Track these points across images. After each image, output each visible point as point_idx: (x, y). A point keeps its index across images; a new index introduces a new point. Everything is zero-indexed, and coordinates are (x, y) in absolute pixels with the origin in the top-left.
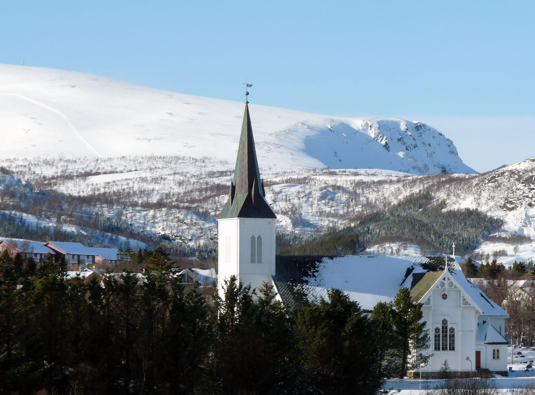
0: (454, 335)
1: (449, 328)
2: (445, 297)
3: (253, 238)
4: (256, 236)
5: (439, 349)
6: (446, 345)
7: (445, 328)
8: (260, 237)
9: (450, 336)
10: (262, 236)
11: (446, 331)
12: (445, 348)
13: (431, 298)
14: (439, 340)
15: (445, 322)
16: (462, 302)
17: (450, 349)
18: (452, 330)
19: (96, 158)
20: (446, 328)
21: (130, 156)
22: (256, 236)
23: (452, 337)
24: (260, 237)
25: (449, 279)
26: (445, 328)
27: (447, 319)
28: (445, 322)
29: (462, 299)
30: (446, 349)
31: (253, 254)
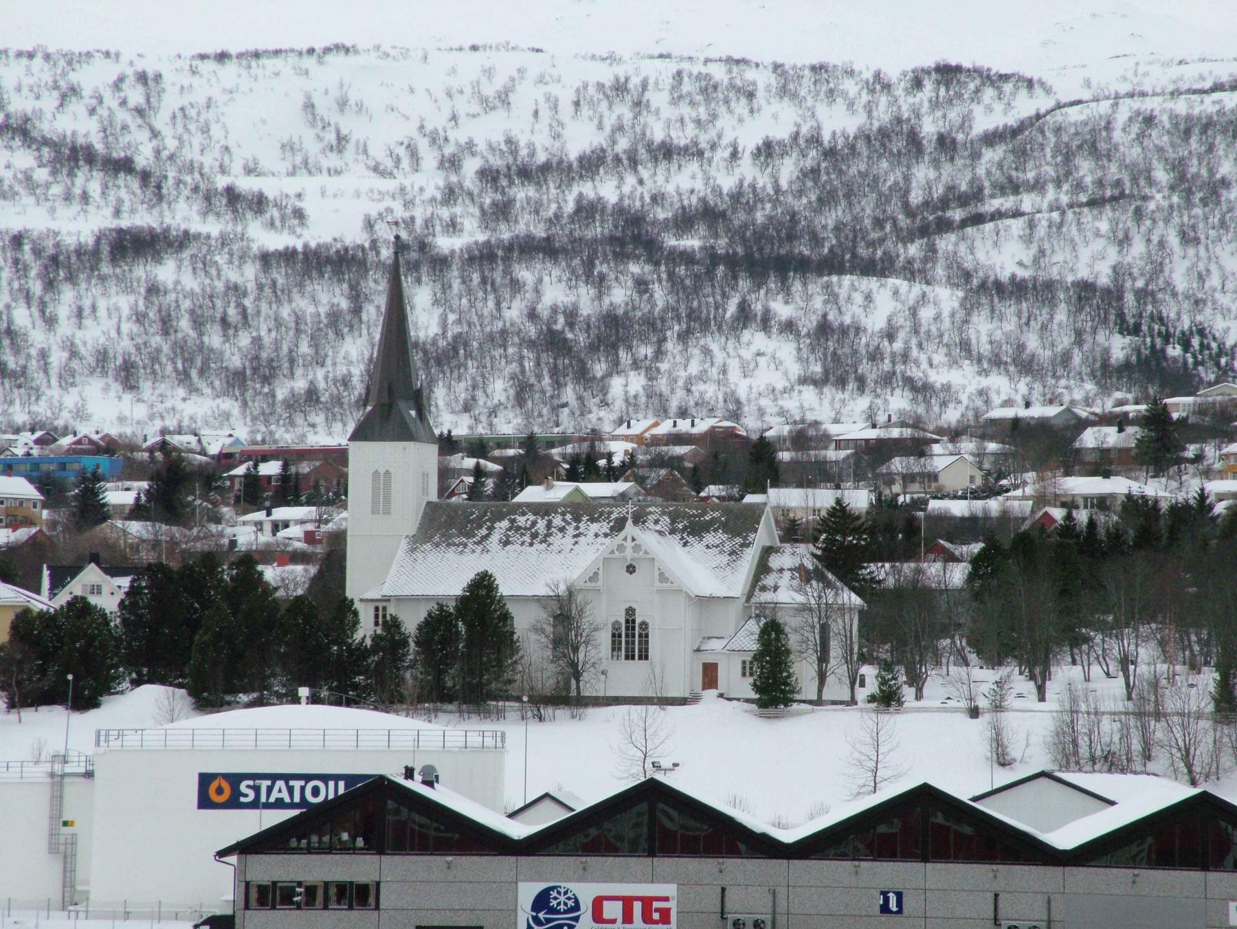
0: (647, 636)
1: (638, 621)
2: (631, 569)
3: (376, 473)
4: (382, 471)
5: (633, 658)
6: (633, 651)
7: (630, 623)
8: (387, 473)
9: (640, 636)
10: (391, 470)
11: (633, 628)
12: (630, 657)
13: (600, 572)
14: (633, 642)
15: (630, 612)
16: (657, 577)
17: (640, 658)
18: (644, 625)
19: (755, 114)
20: (634, 621)
21: (989, 70)
22: (382, 471)
23: (645, 637)
24: (387, 473)
25: (633, 540)
26: (630, 623)
27: (634, 606)
28: (630, 612)
29: (657, 573)
30: (633, 658)
31: (375, 502)
